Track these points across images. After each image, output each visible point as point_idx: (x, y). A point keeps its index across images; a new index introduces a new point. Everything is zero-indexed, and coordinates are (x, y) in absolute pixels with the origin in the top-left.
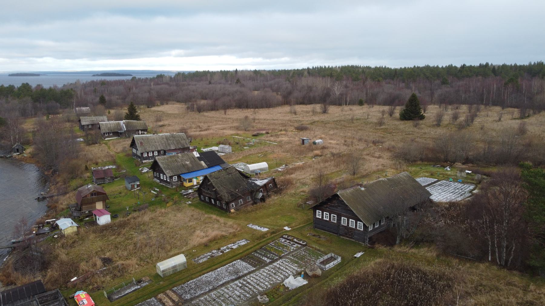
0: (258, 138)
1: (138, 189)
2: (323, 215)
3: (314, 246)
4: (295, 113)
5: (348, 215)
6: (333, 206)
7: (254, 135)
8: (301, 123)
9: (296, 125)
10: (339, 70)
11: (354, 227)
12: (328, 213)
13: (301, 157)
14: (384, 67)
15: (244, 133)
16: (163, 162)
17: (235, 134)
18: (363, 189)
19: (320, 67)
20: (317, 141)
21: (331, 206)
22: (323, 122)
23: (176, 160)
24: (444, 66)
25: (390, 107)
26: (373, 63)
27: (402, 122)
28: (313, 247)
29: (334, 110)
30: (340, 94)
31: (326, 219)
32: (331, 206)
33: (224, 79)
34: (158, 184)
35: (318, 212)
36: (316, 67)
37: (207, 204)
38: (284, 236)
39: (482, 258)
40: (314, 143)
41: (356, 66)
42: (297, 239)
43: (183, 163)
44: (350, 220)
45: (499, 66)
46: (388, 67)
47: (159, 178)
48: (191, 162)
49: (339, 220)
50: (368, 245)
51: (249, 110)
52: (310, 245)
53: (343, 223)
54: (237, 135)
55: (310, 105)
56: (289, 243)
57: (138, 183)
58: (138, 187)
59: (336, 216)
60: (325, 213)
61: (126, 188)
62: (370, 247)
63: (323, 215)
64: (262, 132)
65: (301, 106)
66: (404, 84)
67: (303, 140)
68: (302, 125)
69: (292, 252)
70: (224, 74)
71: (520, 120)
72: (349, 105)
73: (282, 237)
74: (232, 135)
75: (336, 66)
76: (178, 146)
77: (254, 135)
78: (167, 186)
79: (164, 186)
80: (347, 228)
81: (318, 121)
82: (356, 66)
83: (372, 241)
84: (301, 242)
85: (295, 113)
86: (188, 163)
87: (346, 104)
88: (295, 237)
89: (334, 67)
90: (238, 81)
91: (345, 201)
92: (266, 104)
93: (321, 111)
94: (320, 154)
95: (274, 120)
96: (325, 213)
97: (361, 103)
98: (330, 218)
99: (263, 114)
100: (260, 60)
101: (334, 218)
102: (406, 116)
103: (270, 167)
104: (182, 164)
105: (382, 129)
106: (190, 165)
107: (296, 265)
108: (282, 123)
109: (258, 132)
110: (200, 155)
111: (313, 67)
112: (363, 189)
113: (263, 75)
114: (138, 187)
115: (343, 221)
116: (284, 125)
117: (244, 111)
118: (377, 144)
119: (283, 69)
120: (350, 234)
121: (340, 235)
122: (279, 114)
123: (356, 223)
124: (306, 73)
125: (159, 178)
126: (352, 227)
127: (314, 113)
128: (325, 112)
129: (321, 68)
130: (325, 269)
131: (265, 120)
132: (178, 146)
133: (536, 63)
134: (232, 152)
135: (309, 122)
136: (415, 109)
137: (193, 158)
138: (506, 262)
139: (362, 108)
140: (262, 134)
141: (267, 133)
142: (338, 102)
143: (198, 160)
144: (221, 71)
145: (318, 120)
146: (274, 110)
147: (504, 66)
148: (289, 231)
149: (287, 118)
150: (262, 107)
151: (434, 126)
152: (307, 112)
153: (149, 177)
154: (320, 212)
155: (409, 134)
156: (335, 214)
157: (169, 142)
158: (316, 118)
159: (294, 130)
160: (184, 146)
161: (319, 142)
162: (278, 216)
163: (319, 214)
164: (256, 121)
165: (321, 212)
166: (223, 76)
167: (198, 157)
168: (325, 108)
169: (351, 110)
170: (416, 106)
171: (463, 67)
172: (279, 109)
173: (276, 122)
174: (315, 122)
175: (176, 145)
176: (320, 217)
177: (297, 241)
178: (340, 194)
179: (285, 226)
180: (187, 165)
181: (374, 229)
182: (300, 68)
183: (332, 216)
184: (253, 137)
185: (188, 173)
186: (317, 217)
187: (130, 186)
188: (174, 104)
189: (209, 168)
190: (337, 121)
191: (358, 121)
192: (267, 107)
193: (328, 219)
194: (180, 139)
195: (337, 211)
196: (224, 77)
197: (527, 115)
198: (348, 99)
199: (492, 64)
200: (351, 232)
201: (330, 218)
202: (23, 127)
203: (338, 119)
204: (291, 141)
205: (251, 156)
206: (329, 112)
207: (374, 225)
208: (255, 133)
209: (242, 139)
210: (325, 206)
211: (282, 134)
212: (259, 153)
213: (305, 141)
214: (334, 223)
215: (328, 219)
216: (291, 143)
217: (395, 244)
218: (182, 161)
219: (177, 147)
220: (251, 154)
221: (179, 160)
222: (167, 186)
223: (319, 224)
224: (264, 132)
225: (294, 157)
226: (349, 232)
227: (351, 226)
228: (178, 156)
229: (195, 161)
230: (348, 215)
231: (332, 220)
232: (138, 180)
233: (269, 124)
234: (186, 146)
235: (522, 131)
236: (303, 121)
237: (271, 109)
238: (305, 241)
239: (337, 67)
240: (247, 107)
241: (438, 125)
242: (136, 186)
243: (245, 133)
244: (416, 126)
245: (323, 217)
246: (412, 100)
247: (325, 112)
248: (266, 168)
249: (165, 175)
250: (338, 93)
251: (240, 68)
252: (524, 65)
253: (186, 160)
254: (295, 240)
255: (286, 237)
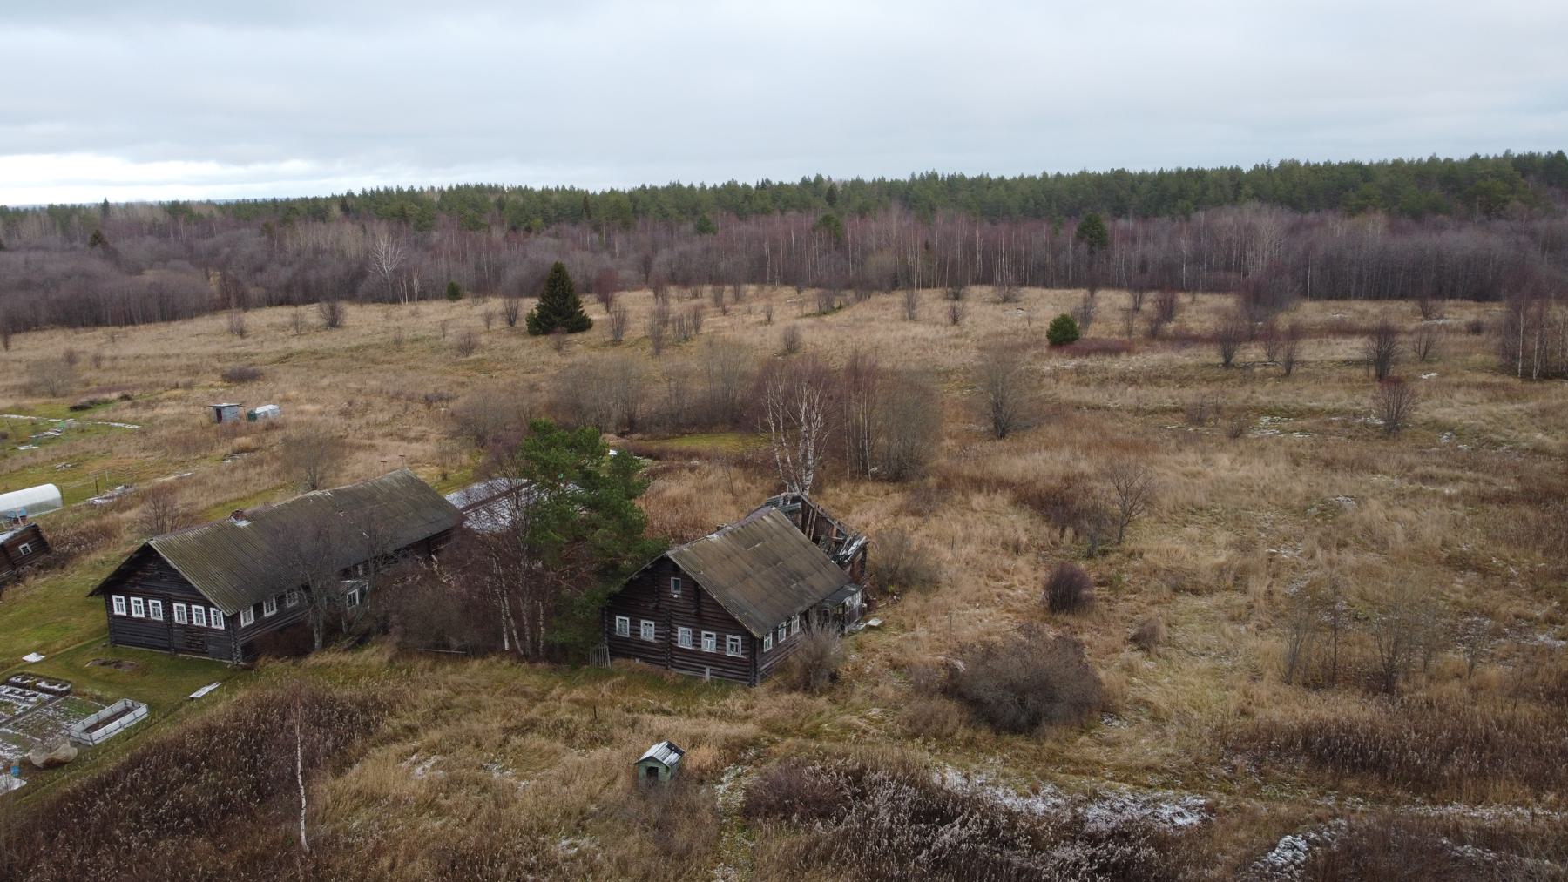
0: (86, 415)
2: (128, 605)
3: (88, 690)
4: (242, 333)
5: (185, 595)
6: (150, 579)
7: (75, 408)
8: (250, 362)
9: (230, 366)
10: (437, 199)
11: (204, 624)
12: (141, 599)
13: (193, 457)
14: (567, 188)
17: (11, 408)
18: (243, 524)
19: (386, 189)
20: (259, 410)
21: (145, 579)
22: (315, 353)
24: (719, 185)
25: (507, 301)
26: (539, 177)
27: (530, 340)
28: (86, 694)
29: (363, 319)
30: (395, 271)
31: (138, 615)
32: (145, 579)
33: (59, 234)
35: (118, 600)
36: (1263, 165)
38: (13, 679)
39: (485, 648)
40: (252, 417)
41: (490, 185)
42: (50, 681)
44: (194, 607)
45: (845, 184)
46: (654, 184)
49: (168, 611)
50: (242, 663)
51: (100, 332)
52: (79, 690)
53: (179, 618)
54: (19, 410)
55: (307, 306)
56: (21, 694)
59: (159, 602)
60: (132, 599)
62: (244, 668)
63: (128, 605)
64: (107, 396)
66: (596, 236)
67: (219, 411)
68: (251, 365)
69: (20, 716)
70: (61, 217)
72: (420, 299)
73: (7, 683)
75: (913, 175)
77: (75, 408)
80: (189, 629)
81: (300, 353)
82: (520, 187)
83: (252, 652)
84: (56, 688)
85: (242, 333)
87: (411, 299)
88: (41, 678)
89: (425, 189)
90: (97, 239)
91: (169, 561)
92: (167, 309)
93: (323, 322)
94: (253, 446)
95: (168, 356)
96: (132, 599)
97: (454, 294)
98: (147, 612)
99: (143, 342)
100: (211, 168)
101: (156, 609)
102: (541, 325)
103: (65, 498)
105: (469, 362)
107: (15, 747)
108: (188, 366)
109: (92, 397)
111: (364, 191)
112: (243, 524)
113: (200, 216)
115: (179, 613)
116: (193, 370)
117: (82, 336)
118: (434, 404)
119: (269, 196)
120: (198, 642)
121: (177, 651)
122: (194, 339)
123: (207, 613)
124: (336, 210)
126: (199, 624)
127: (298, 326)
128: (333, 323)
129: (388, 192)
130: (92, 741)
131: (138, 357)
133: (924, 174)
135: (275, 356)
138: (535, 643)
139: (452, 307)
142: (390, 294)
144: (51, 207)
145: (302, 348)
146: (182, 327)
147: (858, 185)
148: (36, 663)
149: (212, 349)
150: (147, 319)
151: (605, 344)
152: (283, 328)
154: (121, 600)
155: (534, 371)
158: (297, 345)
161: (265, 412)
162: (24, 630)
163: (119, 606)
164: (106, 364)
165: (123, 597)
166: (54, 225)
168: (333, 309)
169: (414, 314)
170: (566, 296)
171: (765, 186)
172: (204, 324)
173: (172, 362)
174: (292, 355)
176: (124, 614)
177: (47, 686)
178: (159, 544)
179: (28, 653)
181: (260, 621)
182: (325, 193)
183: (175, 608)
184: (71, 414)
186: (116, 612)
188: (1466, 307)
190: (357, 348)
191: (418, 345)
192: (163, 320)
193: (143, 616)
195: (160, 588)
196: (58, 228)
197: (836, 305)
199: (830, 179)
200: (199, 637)
201: (147, 612)
203: (362, 343)
204: (183, 417)
205: (30, 471)
206: (349, 322)
207: (258, 609)
209: (29, 423)
210: (131, 581)
211: (169, 399)
212: (61, 460)
213: (225, 413)
215: (143, 616)
216: (182, 421)
217: (312, 648)
220: (29, 466)
223: (123, 632)
224: (115, 395)
225: (170, 461)
226: (196, 639)
227: (198, 621)
230: (185, 595)
231: (152, 614)
233: (145, 372)
236: (257, 354)
237: (175, 324)
238: (70, 682)
239: (436, 190)
240: (98, 322)
241: (616, 342)
243: (50, 403)
244: (558, 348)
245: (129, 611)
246: (555, 281)
247: (333, 323)
248: (54, 500)
250: (387, 268)
251: (118, 197)
252: (288, 199)
254: (43, 684)
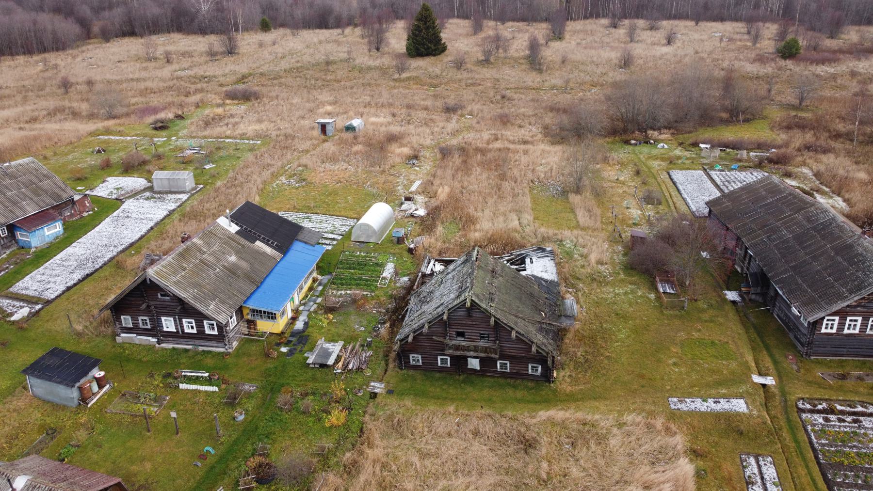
1: (105, 393)
15: (116, 125)
16: (179, 281)
22: (262, 74)
23: (201, 261)
34: (150, 348)
35: (851, 320)
37: (438, 375)
40: (350, 129)
42: (863, 404)
43: (226, 264)
47: (156, 331)
48: (238, 253)
54: (108, 131)
57: (98, 373)
58: (101, 387)
61: (57, 407)
64: (162, 115)
65: (126, 40)
67: (323, 127)
71: (473, 38)
74: (92, 134)
76: (44, 202)
78: (201, 349)
79: (187, 350)
86: (233, 258)
104: (224, 266)
105: (408, 79)
106: (244, 265)
110: (240, 226)
114: (101, 387)
125: (156, 331)
128: (231, 51)
132: (44, 202)
134: (196, 184)
135: (233, 78)
136: (433, 34)
137: (229, 237)
140: (171, 121)
141: (180, 117)
143: (248, 243)
153: (79, 334)
154: (833, 320)
156: (859, 316)
157: (9, 194)
159: (228, 101)
160: (59, 196)
167: (237, 233)
174: (244, 77)
175: (35, 199)
180: (234, 264)
185: (255, 291)
187: (74, 394)
189: (285, 255)
192: (57, 50)
194: (35, 180)
198: (240, 20)
202: (835, 407)
208: (151, 119)
214: (855, 334)
218: (218, 260)
219: (41, 204)
221: (211, 259)
222: (201, 349)
228: (193, 243)
229: (243, 246)
232: (95, 363)
233: (144, 93)
234: (65, 197)
235: (626, 62)
242: (95, 388)
247: (231, 51)
249: (208, 318)
253: (224, 253)
255: (808, 406)
